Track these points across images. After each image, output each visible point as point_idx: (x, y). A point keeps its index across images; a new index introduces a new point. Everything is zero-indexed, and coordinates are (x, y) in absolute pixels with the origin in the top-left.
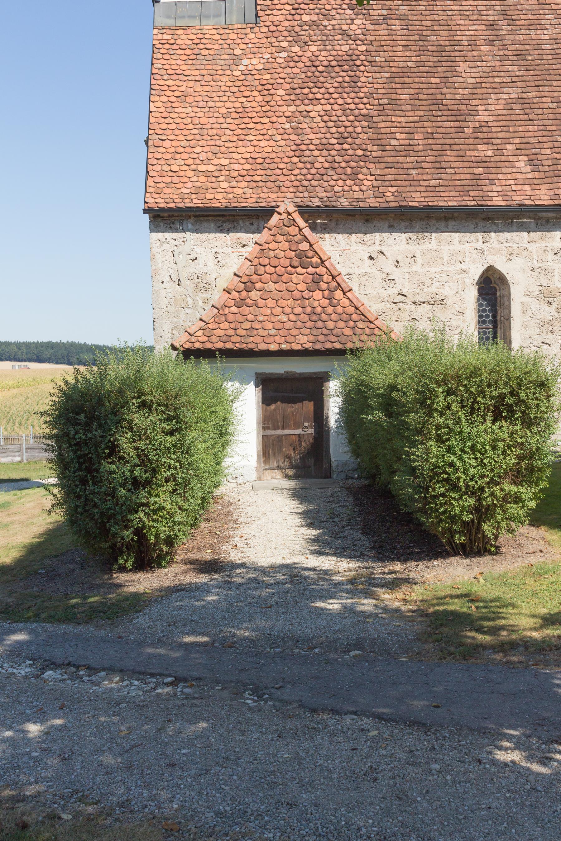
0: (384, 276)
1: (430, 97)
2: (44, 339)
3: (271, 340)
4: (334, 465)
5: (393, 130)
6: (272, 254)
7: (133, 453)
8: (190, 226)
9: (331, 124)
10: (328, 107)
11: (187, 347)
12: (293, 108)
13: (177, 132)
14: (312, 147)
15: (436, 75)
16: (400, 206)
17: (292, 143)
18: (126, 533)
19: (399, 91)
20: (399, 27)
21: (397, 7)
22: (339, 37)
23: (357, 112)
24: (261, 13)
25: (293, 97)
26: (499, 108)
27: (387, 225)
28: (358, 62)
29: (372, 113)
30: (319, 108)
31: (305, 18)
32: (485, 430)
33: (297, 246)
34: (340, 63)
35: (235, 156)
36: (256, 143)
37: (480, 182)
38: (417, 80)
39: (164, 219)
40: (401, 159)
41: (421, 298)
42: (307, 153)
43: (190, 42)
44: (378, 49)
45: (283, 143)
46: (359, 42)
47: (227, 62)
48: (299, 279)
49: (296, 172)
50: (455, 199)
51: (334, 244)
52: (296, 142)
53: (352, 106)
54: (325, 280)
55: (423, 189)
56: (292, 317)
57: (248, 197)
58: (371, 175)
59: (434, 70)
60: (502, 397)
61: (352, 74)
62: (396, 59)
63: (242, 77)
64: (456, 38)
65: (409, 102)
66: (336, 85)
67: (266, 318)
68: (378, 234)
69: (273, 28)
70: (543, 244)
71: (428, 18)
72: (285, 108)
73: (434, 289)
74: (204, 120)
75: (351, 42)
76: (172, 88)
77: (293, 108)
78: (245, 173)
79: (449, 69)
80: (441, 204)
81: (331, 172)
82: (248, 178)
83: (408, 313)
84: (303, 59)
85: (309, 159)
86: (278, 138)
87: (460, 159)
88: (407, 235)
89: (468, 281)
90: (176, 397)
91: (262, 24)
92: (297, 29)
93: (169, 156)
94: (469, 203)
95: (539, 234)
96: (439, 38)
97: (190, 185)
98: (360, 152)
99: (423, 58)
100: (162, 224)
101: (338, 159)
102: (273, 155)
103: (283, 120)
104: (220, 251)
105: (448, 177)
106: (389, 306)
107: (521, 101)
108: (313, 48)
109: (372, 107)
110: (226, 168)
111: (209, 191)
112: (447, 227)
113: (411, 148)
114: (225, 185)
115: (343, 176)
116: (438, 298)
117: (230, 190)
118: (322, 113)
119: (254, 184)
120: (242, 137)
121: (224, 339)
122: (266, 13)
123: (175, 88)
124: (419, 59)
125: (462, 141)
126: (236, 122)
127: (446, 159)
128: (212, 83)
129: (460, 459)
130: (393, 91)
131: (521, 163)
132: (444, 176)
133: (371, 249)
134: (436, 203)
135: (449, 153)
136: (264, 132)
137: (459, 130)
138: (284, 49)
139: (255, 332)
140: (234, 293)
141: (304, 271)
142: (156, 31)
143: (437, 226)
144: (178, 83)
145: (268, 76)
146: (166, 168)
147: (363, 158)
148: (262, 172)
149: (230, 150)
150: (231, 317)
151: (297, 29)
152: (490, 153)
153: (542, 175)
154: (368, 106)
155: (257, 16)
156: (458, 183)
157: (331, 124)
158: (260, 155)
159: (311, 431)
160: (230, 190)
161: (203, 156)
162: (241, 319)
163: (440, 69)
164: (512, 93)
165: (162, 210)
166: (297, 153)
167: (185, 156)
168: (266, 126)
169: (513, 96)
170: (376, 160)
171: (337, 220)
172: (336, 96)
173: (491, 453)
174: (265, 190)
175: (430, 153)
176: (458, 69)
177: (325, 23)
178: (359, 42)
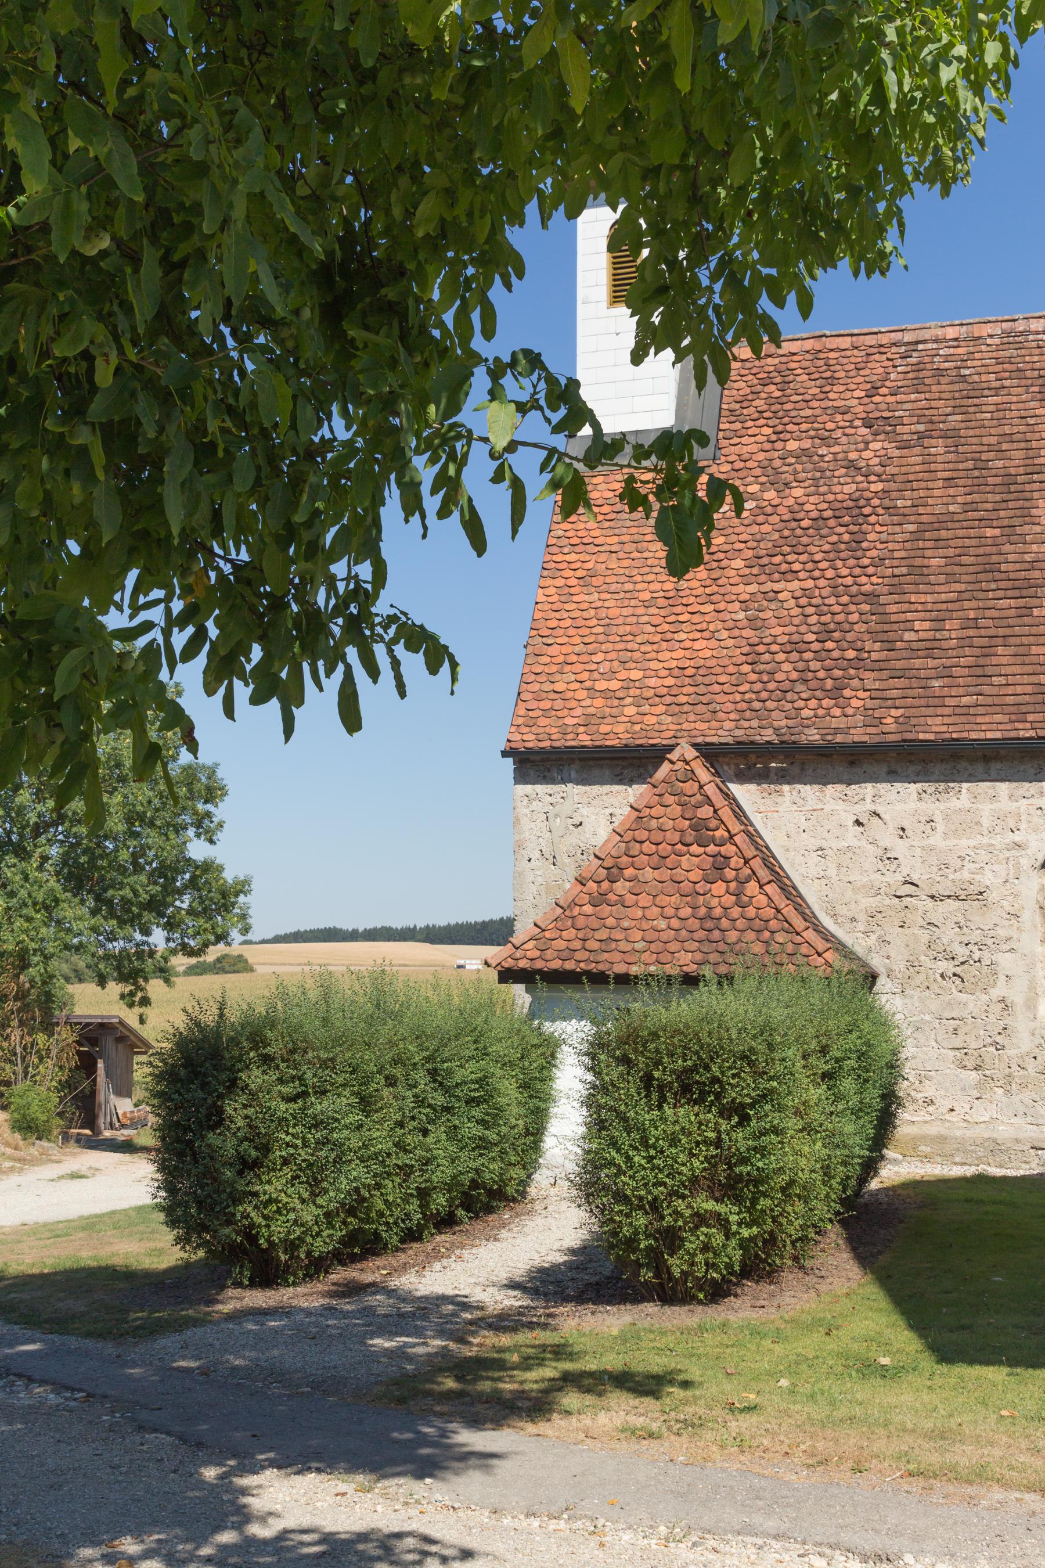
0: (880, 852)
1: (980, 559)
5: (909, 616)
6: (654, 823)
8: (573, 774)
10: (810, 583)
11: (506, 965)
12: (753, 588)
13: (571, 632)
14: (774, 648)
15: (995, 523)
16: (904, 741)
17: (744, 642)
18: (227, 1231)
19: (928, 553)
20: (941, 450)
21: (942, 418)
22: (843, 471)
23: (855, 588)
25: (755, 571)
27: (885, 769)
28: (867, 510)
30: (795, 585)
33: (695, 812)
34: (837, 513)
35: (654, 665)
38: (961, 533)
39: (535, 764)
40: (917, 663)
42: (767, 657)
44: (902, 486)
45: (730, 642)
46: (873, 478)
48: (692, 864)
49: (745, 687)
50: (1000, 727)
51: (797, 800)
52: (751, 641)
53: (849, 581)
54: (732, 865)
55: (947, 711)
56: (675, 923)
57: (617, 733)
58: (865, 690)
59: (993, 515)
61: (856, 528)
62: (930, 501)
64: (1036, 461)
65: (943, 570)
66: (827, 547)
67: (634, 923)
68: (869, 785)
69: (739, 465)
71: (993, 431)
72: (741, 588)
73: (966, 875)
75: (860, 478)
76: (573, 566)
77: (753, 588)
78: (664, 691)
79: (1018, 512)
80: (974, 736)
81: (800, 687)
82: (668, 700)
83: (920, 913)
84: (781, 510)
85: (768, 667)
86: (725, 634)
87: (1019, 660)
88: (919, 785)
91: (723, 459)
92: (777, 463)
94: (1022, 734)
96: (1007, 463)
97: (578, 712)
98: (851, 654)
99: (976, 497)
100: (532, 772)
101: (814, 665)
102: (713, 662)
105: (994, 690)
106: (887, 902)
108: (798, 492)
109: (880, 580)
110: (637, 684)
111: (605, 721)
112: (987, 772)
113: (936, 644)
114: (631, 711)
115: (818, 694)
116: (974, 889)
117: (638, 718)
118: (798, 594)
119: (676, 709)
120: (669, 636)
121: (565, 954)
122: (732, 442)
123: (578, 565)
124: (969, 498)
125: (1026, 630)
126: (663, 612)
127: (994, 660)
130: (919, 553)
132: (986, 689)
133: (859, 808)
134: (965, 735)
135: (1000, 650)
136: (704, 626)
137: (1024, 611)
139: (613, 945)
140: (591, 884)
141: (701, 850)
144: (582, 557)
146: (547, 687)
147: (854, 663)
148: (692, 690)
149: (648, 656)
150: (581, 922)
151: (777, 463)
154: (874, 579)
157: (811, 610)
158: (692, 663)
160: (638, 718)
163: (1002, 513)
165: (530, 751)
166: (750, 659)
167: (578, 668)
168: (707, 618)
170: (877, 665)
171: (803, 763)
172: (824, 565)
174: (692, 717)
175: (968, 651)
176: (1034, 512)
178: (873, 478)
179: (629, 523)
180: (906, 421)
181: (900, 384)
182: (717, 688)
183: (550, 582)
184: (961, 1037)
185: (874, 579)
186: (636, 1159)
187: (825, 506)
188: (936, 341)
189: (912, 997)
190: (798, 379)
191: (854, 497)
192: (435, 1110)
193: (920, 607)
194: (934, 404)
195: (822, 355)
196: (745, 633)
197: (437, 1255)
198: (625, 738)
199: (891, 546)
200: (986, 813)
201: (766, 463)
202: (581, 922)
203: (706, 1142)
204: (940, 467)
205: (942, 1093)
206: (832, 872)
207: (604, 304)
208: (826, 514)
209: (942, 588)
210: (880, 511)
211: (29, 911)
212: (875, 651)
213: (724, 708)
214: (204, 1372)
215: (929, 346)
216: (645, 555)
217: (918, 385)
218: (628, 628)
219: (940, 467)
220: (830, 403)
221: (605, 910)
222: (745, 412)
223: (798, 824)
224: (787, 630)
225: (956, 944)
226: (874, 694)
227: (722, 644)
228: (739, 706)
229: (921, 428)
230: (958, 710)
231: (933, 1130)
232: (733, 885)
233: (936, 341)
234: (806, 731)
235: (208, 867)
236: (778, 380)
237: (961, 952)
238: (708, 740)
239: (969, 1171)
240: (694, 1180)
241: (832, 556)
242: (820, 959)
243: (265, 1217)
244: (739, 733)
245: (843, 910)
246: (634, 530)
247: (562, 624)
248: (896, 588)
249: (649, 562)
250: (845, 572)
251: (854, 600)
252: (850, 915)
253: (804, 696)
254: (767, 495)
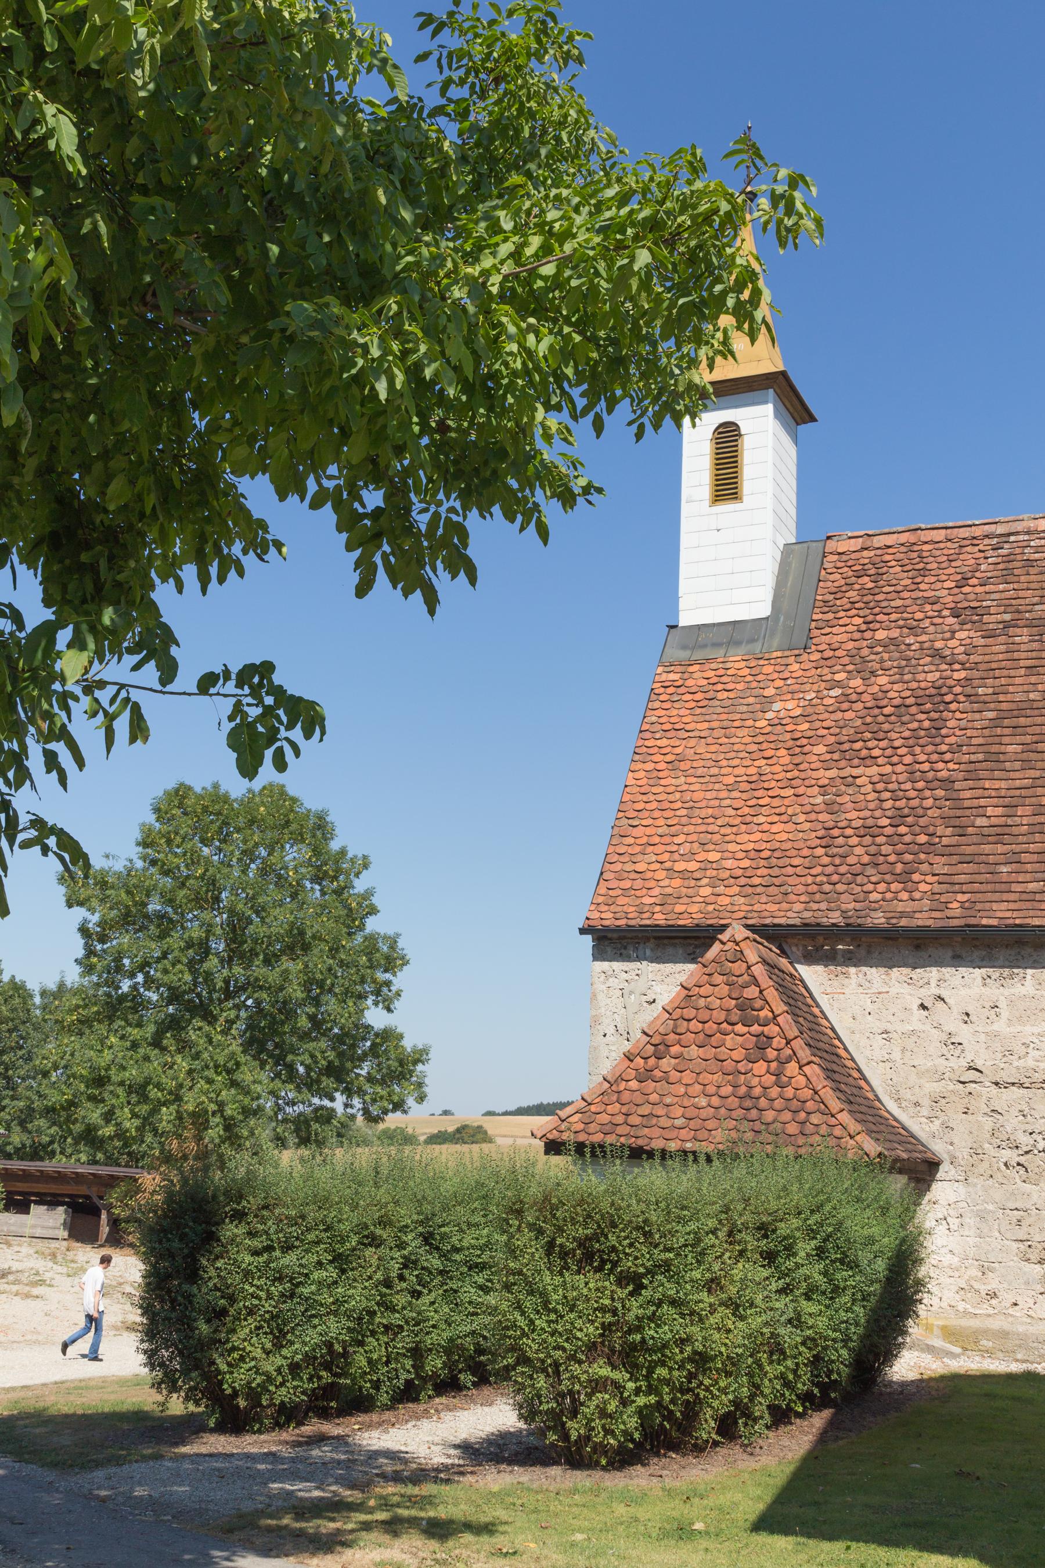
0: (945, 1037)
5: (982, 802)
6: (702, 1002)
8: (648, 952)
10: (888, 769)
11: (550, 1136)
14: (849, 832)
16: (968, 926)
19: (1006, 740)
20: (1025, 639)
21: (1029, 608)
22: (928, 659)
25: (836, 756)
27: (950, 954)
28: (948, 698)
30: (875, 770)
33: (741, 992)
34: (919, 701)
35: (732, 847)
39: (613, 942)
40: (987, 848)
41: (1004, 1077)
43: (705, 682)
47: (750, 709)
49: (818, 870)
52: (827, 825)
53: (926, 767)
56: (715, 1101)
57: (690, 913)
62: (1011, 689)
63: (769, 729)
65: (1019, 757)
66: (907, 734)
68: (934, 969)
69: (829, 654)
72: (821, 773)
73: (1030, 1063)
75: (944, 667)
76: (664, 751)
78: (740, 872)
81: (870, 871)
82: (743, 881)
83: (984, 1099)
86: (802, 818)
88: (983, 970)
91: (814, 648)
92: (865, 652)
93: (638, 849)
97: (656, 891)
100: (609, 949)
101: (886, 849)
106: (951, 1087)
108: (883, 680)
110: (714, 866)
111: (681, 901)
113: (1007, 830)
114: (706, 891)
115: (888, 877)
117: (712, 899)
118: (875, 779)
119: (750, 890)
120: (748, 819)
121: (607, 1128)
126: (744, 796)
128: (724, 740)
130: (997, 740)
134: (1028, 921)
136: (782, 810)
139: (654, 1121)
140: (638, 1060)
141: (746, 1029)
142: (660, 670)
143: (1035, 957)
144: (673, 742)
146: (629, 867)
148: (765, 872)
149: (727, 838)
150: (626, 1097)
151: (865, 652)
154: (951, 766)
160: (712, 899)
165: (606, 929)
166: (824, 842)
168: (787, 802)
170: (947, 850)
171: (870, 946)
172: (903, 751)
174: (764, 899)
178: (957, 666)
179: (719, 710)
180: (993, 610)
181: (989, 574)
182: (790, 870)
183: (640, 766)
184: (1025, 1228)
185: (951, 766)
186: (537, 1322)
187: (908, 693)
188: (1028, 533)
189: (975, 1185)
190: (891, 570)
191: (937, 684)
192: (430, 1273)
193: (993, 793)
194: (1021, 594)
195: (916, 548)
196: (821, 817)
197: (426, 1415)
199: (969, 733)
201: (854, 652)
202: (626, 1097)
203: (603, 1309)
204: (1023, 655)
205: (1005, 1285)
206: (896, 1055)
207: (707, 503)
208: (909, 701)
209: (1017, 775)
210: (962, 698)
211: (210, 1073)
212: (946, 835)
213: (796, 890)
215: (1021, 538)
216: (732, 740)
218: (710, 811)
219: (1023, 655)
220: (921, 594)
221: (650, 1085)
222: (838, 602)
223: (862, 1005)
224: (862, 814)
225: (1020, 1132)
226: (942, 878)
227: (799, 827)
228: (810, 889)
229: (1007, 617)
230: (1024, 896)
231: (995, 1324)
232: (774, 1065)
233: (1028, 533)
234: (873, 914)
235: (388, 1035)
236: (872, 572)
237: (1025, 1141)
238: (776, 921)
239: (1015, 1368)
240: (592, 1347)
241: (911, 742)
242: (852, 1142)
243: (229, 1364)
244: (807, 914)
245: (907, 1095)
246: (724, 717)
247: (649, 806)
248: (971, 775)
249: (736, 747)
250: (922, 758)
251: (930, 785)
252: (914, 1099)
253: (873, 879)
254: (853, 683)
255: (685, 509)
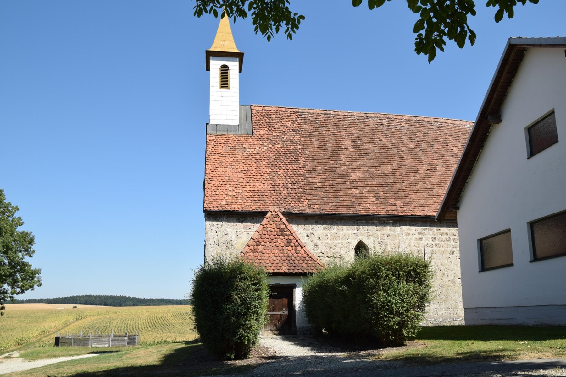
2: (109, 294)
3: (270, 268)
4: (298, 328)
7: (239, 300)
9: (288, 177)
10: (286, 170)
12: (270, 170)
13: (218, 178)
14: (279, 187)
24: (254, 131)
25: (270, 166)
26: (360, 174)
28: (298, 153)
29: (305, 174)
30: (282, 170)
31: (274, 134)
32: (404, 286)
35: (245, 189)
36: (254, 184)
37: (355, 204)
39: (212, 215)
40: (320, 193)
42: (278, 189)
45: (267, 184)
48: (281, 241)
53: (297, 171)
56: (279, 258)
57: (252, 207)
60: (409, 272)
69: (260, 137)
70: (383, 232)
72: (267, 170)
73: (336, 251)
74: (230, 173)
77: (270, 170)
81: (289, 198)
82: (251, 199)
86: (264, 182)
89: (351, 247)
90: (258, 274)
92: (271, 138)
93: (215, 188)
95: (381, 227)
97: (224, 201)
98: (301, 190)
102: (263, 189)
103: (266, 175)
104: (238, 231)
107: (368, 172)
108: (278, 146)
114: (241, 201)
129: (393, 298)
131: (371, 197)
133: (308, 232)
138: (265, 146)
140: (251, 246)
145: (259, 157)
150: (250, 257)
151: (271, 138)
152: (358, 192)
153: (380, 202)
155: (253, 132)
156: (345, 204)
157: (288, 177)
159: (286, 312)
161: (230, 189)
162: (255, 258)
164: (365, 169)
165: (212, 211)
167: (222, 188)
169: (365, 170)
172: (289, 166)
173: (406, 296)
177: (283, 136)
198: (241, 209)
200: (341, 234)
207: (218, 88)
214: (303, 374)
217: (305, 123)
221: (257, 254)
255: (211, 89)
